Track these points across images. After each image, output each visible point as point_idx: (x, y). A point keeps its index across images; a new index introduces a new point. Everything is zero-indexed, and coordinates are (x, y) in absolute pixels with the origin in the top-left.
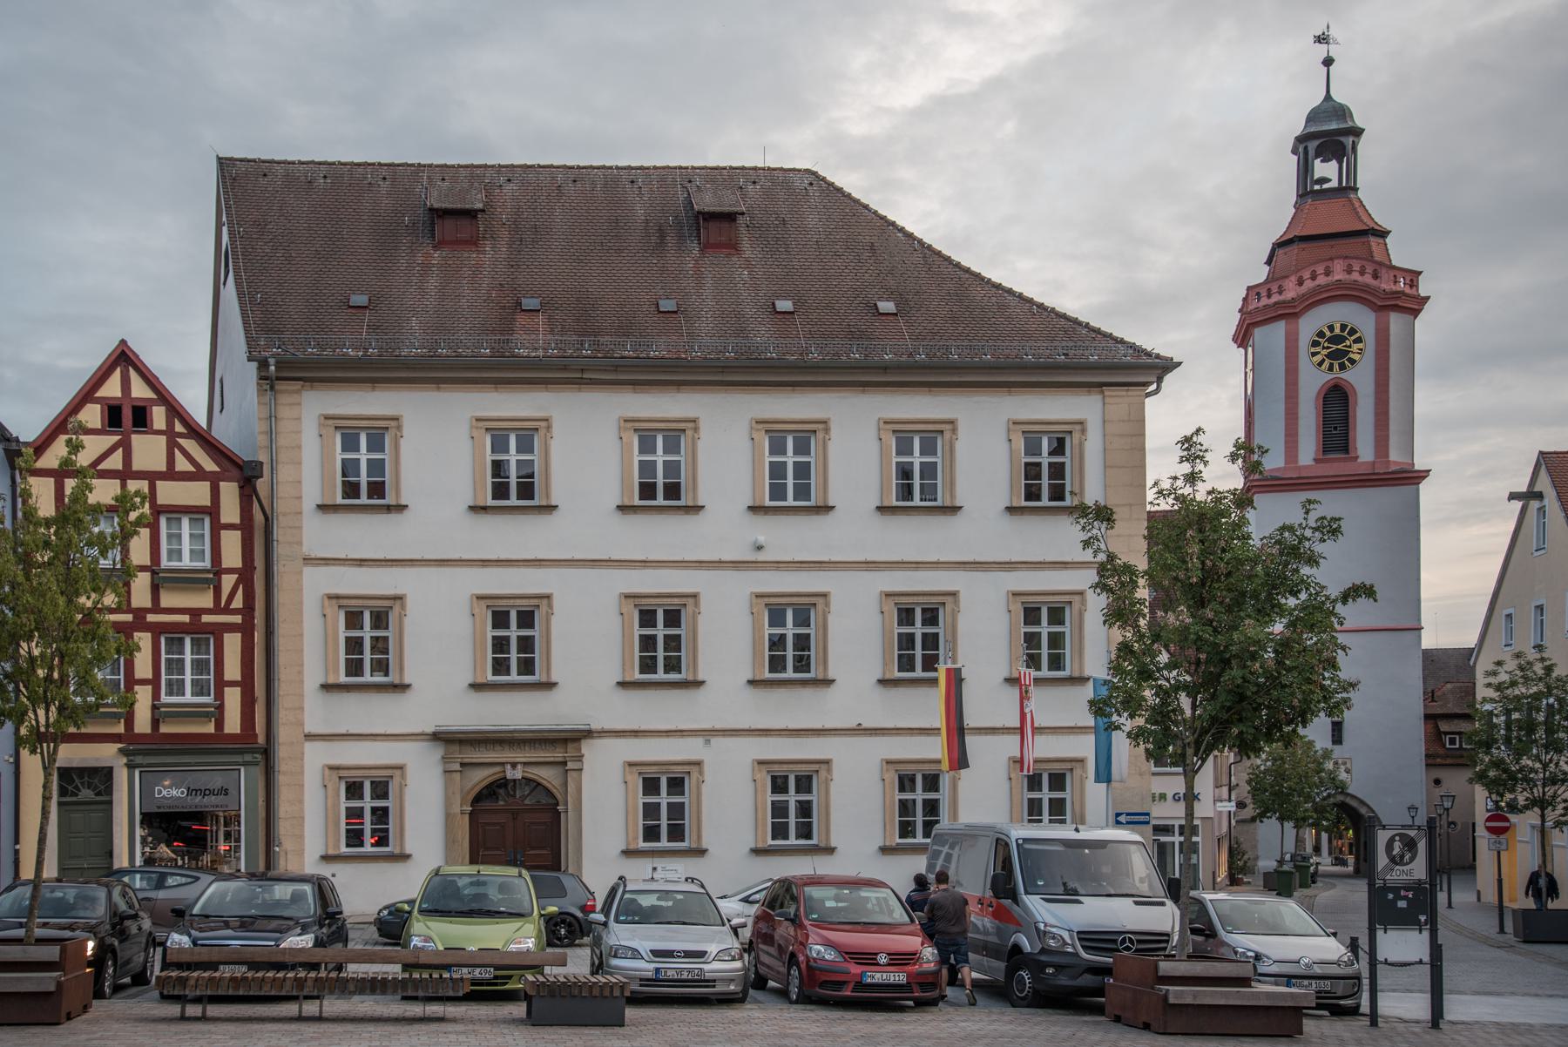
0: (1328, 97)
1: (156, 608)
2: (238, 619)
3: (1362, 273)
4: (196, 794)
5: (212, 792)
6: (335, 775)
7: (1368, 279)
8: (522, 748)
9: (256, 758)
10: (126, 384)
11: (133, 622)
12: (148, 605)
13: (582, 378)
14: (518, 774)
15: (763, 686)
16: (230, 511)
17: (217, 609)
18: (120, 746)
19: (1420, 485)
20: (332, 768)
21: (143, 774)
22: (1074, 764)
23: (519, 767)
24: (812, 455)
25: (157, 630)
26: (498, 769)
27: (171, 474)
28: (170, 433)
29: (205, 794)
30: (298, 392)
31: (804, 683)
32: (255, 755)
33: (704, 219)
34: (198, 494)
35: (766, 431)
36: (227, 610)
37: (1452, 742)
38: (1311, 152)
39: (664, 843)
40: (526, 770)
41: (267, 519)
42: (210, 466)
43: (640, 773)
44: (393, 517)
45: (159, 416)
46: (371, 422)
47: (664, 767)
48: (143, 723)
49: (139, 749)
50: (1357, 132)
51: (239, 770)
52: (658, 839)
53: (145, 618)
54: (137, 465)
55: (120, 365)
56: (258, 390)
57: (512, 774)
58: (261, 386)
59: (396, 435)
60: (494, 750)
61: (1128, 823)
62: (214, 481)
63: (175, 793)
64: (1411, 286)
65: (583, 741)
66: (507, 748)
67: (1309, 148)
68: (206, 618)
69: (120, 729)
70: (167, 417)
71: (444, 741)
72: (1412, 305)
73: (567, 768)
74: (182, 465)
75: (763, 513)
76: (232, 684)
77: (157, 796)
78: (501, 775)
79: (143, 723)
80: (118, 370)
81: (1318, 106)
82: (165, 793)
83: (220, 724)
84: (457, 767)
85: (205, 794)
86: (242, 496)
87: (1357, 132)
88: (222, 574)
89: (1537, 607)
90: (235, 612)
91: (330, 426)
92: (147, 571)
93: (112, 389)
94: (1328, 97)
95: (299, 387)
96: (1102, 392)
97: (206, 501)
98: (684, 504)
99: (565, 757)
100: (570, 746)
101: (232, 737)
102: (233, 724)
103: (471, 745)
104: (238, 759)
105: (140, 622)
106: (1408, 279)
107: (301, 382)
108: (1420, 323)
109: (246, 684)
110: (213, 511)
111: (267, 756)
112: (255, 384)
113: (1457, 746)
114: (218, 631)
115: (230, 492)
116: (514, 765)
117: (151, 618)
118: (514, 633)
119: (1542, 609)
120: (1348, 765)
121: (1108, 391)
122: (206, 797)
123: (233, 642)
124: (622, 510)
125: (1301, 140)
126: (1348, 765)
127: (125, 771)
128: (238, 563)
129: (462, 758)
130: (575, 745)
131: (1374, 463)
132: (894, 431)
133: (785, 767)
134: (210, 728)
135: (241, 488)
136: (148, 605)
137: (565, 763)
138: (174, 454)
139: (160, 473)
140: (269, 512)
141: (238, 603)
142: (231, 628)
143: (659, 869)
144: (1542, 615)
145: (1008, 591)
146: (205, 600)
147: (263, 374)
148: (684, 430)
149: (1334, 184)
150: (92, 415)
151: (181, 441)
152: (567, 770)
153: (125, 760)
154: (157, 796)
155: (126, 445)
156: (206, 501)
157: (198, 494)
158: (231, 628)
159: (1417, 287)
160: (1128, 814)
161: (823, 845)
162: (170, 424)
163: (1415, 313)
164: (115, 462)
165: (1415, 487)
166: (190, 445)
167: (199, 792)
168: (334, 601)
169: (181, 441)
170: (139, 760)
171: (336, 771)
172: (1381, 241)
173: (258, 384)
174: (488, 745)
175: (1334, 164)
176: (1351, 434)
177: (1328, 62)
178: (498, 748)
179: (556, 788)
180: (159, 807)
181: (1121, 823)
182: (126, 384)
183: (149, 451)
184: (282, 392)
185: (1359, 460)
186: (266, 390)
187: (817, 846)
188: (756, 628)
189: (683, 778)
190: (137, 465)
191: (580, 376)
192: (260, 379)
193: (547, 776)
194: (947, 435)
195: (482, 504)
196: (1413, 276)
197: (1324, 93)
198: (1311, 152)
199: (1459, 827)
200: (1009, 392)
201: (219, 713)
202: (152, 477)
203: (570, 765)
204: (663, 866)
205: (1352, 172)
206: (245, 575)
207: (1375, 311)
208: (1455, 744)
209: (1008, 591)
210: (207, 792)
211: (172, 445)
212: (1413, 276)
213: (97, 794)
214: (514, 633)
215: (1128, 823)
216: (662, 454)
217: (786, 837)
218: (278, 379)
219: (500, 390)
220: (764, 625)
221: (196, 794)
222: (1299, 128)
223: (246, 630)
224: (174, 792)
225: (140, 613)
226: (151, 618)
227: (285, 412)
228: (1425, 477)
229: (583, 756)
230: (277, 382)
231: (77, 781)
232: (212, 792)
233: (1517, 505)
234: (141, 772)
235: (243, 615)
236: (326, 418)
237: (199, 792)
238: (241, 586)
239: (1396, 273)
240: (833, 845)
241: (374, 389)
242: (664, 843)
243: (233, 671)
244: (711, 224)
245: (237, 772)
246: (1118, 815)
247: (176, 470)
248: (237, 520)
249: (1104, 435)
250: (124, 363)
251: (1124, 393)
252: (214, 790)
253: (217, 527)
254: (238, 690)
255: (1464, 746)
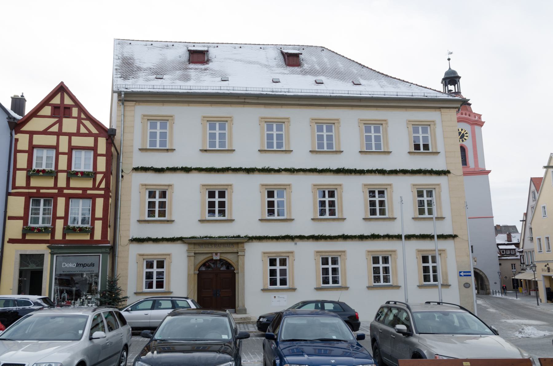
0: (450, 68)
1: (68, 187)
2: (102, 192)
3: (466, 115)
4: (80, 266)
5: (87, 265)
6: (141, 258)
7: (467, 116)
8: (220, 246)
9: (107, 250)
10: (62, 99)
11: (58, 193)
12: (65, 186)
13: (245, 102)
14: (217, 258)
15: (317, 221)
16: (102, 147)
17: (94, 188)
18: (48, 245)
19: (489, 175)
20: (140, 255)
21: (57, 257)
22: (441, 252)
23: (219, 254)
24: (285, 198)
25: (69, 197)
26: (210, 255)
27: (78, 134)
28: (79, 119)
29: (84, 266)
30: (134, 106)
31: (334, 219)
32: (107, 249)
33: (288, 56)
34: (89, 142)
35: (316, 123)
36: (98, 189)
37: (503, 252)
38: (447, 83)
39: (278, 286)
40: (221, 256)
41: (118, 154)
42: (94, 131)
43: (268, 257)
44: (170, 154)
45: (75, 112)
46: (163, 118)
47: (278, 254)
48: (59, 236)
49: (54, 246)
50: (459, 78)
51: (100, 255)
52: (276, 284)
53: (63, 191)
54: (64, 130)
55: (60, 92)
56: (118, 105)
57: (215, 258)
58: (119, 104)
59: (171, 122)
60: (208, 247)
61: (464, 276)
62: (96, 137)
63: (71, 265)
64: (480, 119)
65: (245, 243)
66: (213, 246)
67: (447, 81)
68: (89, 192)
69: (48, 237)
70: (78, 112)
71: (187, 243)
72: (481, 124)
73: (238, 255)
74: (83, 130)
75: (315, 153)
76: (99, 219)
77: (63, 267)
78: (211, 258)
79: (59, 236)
80: (60, 94)
81: (448, 71)
82: (66, 265)
83: (92, 236)
84: (193, 254)
85: (84, 266)
86: (107, 143)
87: (459, 78)
88: (97, 174)
89: (543, 207)
90: (102, 189)
91: (146, 119)
92: (65, 172)
93: (56, 100)
94: (450, 68)
95: (134, 104)
96: (440, 110)
97: (92, 144)
98: (285, 150)
99: (237, 250)
100: (240, 245)
101: (98, 242)
102: (98, 236)
103: (199, 245)
104: (100, 251)
105: (61, 192)
106: (479, 117)
107: (135, 102)
108: (483, 128)
109: (105, 219)
110: (94, 149)
111: (112, 250)
112: (117, 103)
113: (505, 253)
114: (93, 198)
115: (102, 142)
116: (216, 254)
117: (65, 191)
118: (217, 200)
119: (545, 208)
120: (475, 259)
121: (443, 110)
122: (84, 267)
123: (100, 202)
124: (260, 152)
125: (444, 79)
126: (475, 259)
127: (50, 255)
128: (104, 169)
129: (195, 250)
130: (242, 245)
131: (475, 168)
132: (364, 124)
133: (327, 254)
134: (87, 237)
135: (107, 140)
136: (65, 186)
137: (238, 253)
138: (80, 126)
139: (74, 133)
140: (119, 152)
141: (103, 186)
142: (100, 196)
143: (277, 297)
144: (545, 209)
145: (411, 184)
146: (88, 184)
147: (120, 99)
148: (284, 122)
149: (454, 91)
150: (47, 110)
151: (84, 121)
152: (238, 256)
153: (50, 251)
154: (63, 267)
155: (60, 123)
156: (92, 144)
157: (89, 142)
158: (100, 196)
159: (481, 119)
160: (464, 272)
161: (344, 286)
162: (79, 114)
163: (482, 126)
164: (55, 129)
165: (486, 176)
166: (87, 123)
167: (82, 265)
168: (144, 187)
169: (84, 121)
170: (56, 251)
171: (142, 256)
172: (469, 106)
173: (118, 103)
174: (206, 245)
175: (453, 86)
176: (467, 160)
177: (449, 59)
178: (210, 246)
179: (234, 263)
180: (64, 272)
181: (462, 276)
182: (62, 99)
183: (69, 125)
184: (127, 106)
185: (470, 167)
186: (121, 105)
187: (341, 286)
188: (314, 198)
189: (286, 259)
190: (64, 130)
191: (244, 101)
192: (119, 101)
193: (230, 258)
194: (384, 125)
195: (205, 149)
196: (480, 116)
197: (449, 68)
198: (447, 83)
199: (508, 278)
200: (406, 110)
201: (92, 231)
202: (70, 135)
203: (240, 253)
204: (278, 296)
205: (459, 88)
206: (107, 175)
207: (471, 125)
208: (513, 252)
209: (411, 184)
210: (85, 265)
211: (80, 123)
212: (480, 116)
213: (37, 266)
214: (217, 200)
215: (464, 276)
216: (275, 131)
217: (429, 281)
218: (126, 101)
219: (212, 106)
220: (317, 197)
221: (80, 266)
222: (443, 76)
223: (106, 197)
224: (71, 265)
225: (61, 189)
226: (65, 191)
227: (128, 113)
228: (490, 172)
229: (245, 250)
230: (125, 102)
231: (28, 260)
232: (87, 265)
233: (545, 170)
234: (57, 256)
235: (105, 191)
236: (144, 116)
237: (82, 265)
238: (105, 179)
239: (476, 115)
240: (348, 286)
241: (163, 105)
242: (278, 286)
243: (99, 213)
244: (290, 57)
245: (99, 256)
246: (460, 272)
247: (81, 132)
248: (104, 152)
249: (443, 126)
250: (62, 91)
251: (449, 111)
252: (88, 264)
253: (96, 155)
254: (101, 222)
255: (511, 253)
